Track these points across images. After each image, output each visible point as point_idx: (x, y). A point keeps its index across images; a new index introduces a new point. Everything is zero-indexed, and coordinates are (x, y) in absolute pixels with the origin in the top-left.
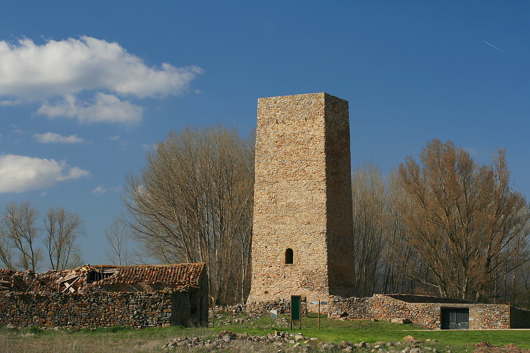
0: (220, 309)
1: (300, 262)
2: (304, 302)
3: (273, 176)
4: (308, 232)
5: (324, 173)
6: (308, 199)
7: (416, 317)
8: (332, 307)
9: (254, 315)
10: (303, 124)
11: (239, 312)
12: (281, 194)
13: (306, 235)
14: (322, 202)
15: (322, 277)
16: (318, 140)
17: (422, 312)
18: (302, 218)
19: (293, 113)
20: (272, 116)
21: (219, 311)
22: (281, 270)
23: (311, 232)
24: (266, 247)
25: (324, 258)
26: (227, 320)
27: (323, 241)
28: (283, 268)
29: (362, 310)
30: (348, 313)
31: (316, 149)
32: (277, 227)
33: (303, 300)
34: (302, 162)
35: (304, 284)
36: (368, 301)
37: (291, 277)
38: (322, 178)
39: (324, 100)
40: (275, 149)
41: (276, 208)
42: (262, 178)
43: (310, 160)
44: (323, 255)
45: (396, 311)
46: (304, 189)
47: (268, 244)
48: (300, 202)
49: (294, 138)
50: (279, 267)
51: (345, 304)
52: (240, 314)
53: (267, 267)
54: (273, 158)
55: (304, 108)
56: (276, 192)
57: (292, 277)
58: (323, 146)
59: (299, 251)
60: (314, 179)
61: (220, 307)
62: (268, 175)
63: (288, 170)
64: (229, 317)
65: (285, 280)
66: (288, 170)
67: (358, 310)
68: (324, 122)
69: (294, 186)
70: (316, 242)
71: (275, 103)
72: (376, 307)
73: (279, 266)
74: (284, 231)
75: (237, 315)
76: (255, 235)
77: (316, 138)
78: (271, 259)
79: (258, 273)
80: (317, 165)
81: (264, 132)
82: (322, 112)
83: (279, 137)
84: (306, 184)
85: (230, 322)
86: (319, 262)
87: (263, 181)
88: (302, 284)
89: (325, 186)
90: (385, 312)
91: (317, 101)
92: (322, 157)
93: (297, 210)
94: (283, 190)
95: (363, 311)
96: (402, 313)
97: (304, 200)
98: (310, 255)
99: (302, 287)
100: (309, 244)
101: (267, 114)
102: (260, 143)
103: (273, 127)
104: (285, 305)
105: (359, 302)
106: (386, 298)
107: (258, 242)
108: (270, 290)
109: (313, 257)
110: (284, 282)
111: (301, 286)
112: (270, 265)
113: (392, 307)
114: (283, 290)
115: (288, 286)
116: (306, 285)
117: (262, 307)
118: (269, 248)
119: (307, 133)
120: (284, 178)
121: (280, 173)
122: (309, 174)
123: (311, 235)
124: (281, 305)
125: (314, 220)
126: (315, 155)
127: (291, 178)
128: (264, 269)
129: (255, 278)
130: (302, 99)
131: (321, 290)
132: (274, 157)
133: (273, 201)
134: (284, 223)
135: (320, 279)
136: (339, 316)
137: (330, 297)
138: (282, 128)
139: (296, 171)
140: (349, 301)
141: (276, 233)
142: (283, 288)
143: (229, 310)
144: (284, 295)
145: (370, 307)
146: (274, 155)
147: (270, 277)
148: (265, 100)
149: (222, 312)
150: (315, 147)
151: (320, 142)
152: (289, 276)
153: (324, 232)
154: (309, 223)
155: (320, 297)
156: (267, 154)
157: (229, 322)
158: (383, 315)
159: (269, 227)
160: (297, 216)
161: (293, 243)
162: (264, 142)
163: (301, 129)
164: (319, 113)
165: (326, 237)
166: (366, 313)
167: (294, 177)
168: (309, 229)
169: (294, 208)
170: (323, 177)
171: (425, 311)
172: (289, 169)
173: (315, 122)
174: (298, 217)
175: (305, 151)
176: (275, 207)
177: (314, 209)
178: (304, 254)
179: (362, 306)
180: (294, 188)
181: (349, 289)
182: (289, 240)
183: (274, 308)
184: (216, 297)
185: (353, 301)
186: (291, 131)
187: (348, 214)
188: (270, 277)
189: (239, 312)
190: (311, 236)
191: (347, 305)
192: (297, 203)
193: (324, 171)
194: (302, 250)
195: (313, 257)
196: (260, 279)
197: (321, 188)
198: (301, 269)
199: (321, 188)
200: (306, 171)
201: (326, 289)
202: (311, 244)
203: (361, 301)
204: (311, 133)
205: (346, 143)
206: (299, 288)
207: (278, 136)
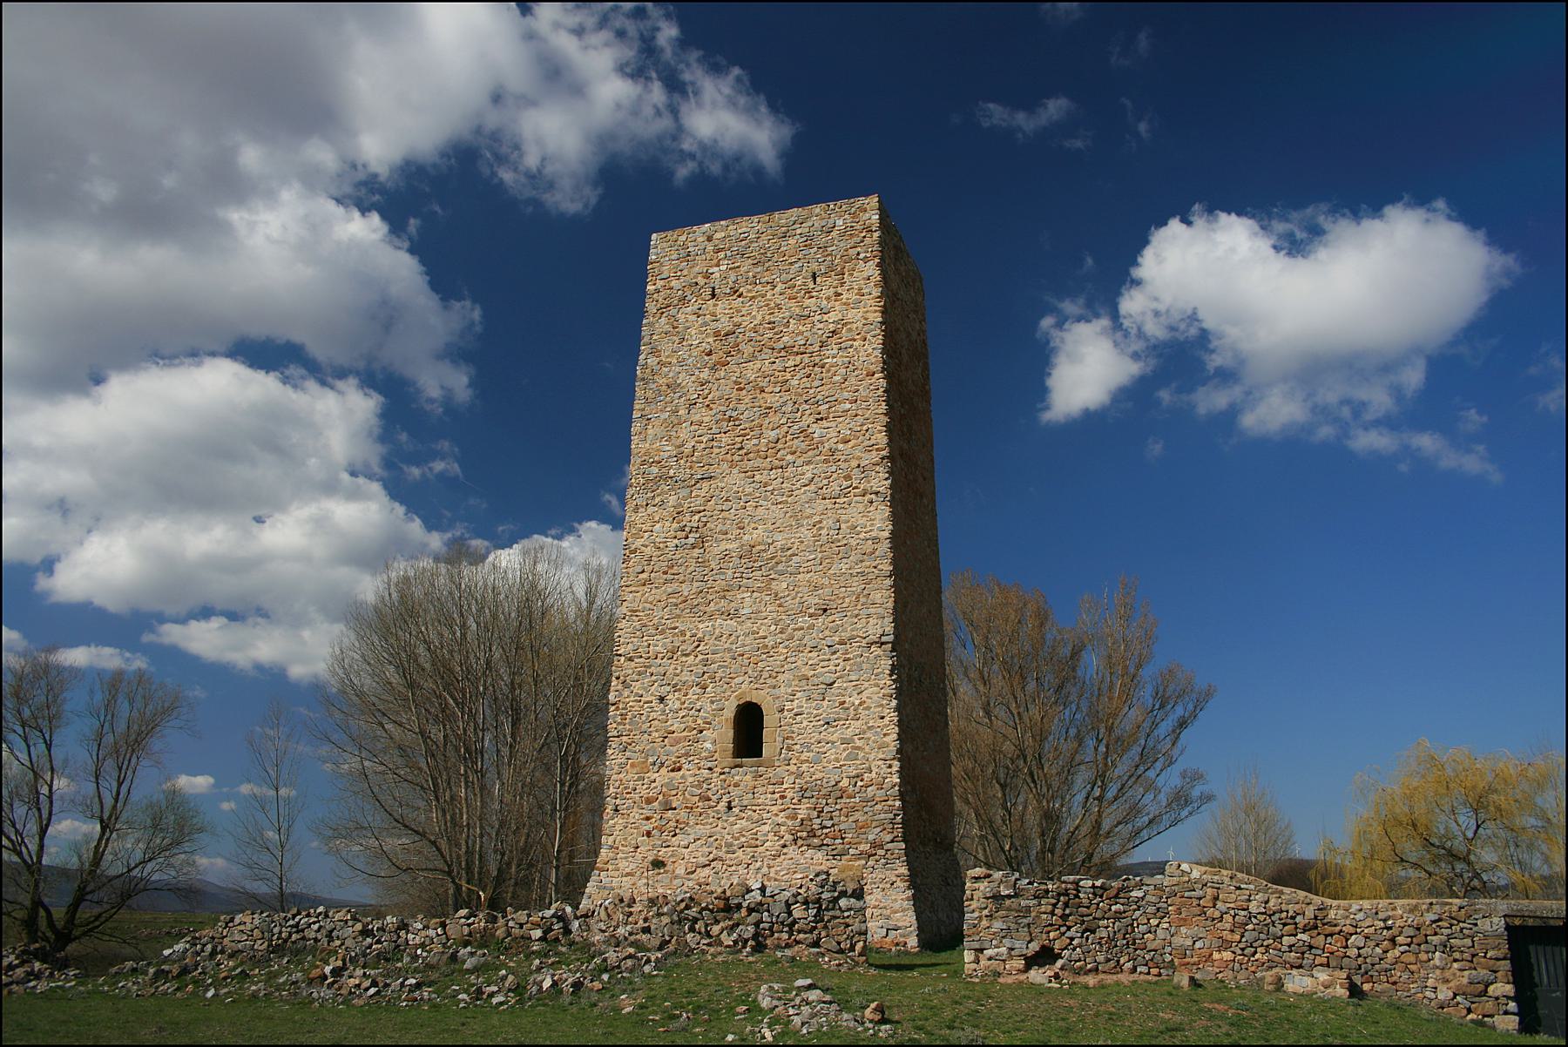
0: (473, 923)
1: (789, 749)
2: (852, 900)
3: (694, 459)
4: (824, 642)
5: (882, 438)
6: (821, 528)
7: (1384, 965)
8: (985, 923)
9: (630, 956)
10: (803, 292)
11: (557, 940)
12: (720, 516)
13: (814, 654)
14: (874, 534)
15: (879, 807)
16: (858, 337)
17: (1412, 942)
18: (799, 595)
19: (770, 263)
20: (695, 277)
21: (470, 934)
22: (716, 780)
23: (834, 640)
24: (662, 699)
25: (885, 735)
26: (504, 978)
27: (881, 673)
28: (724, 773)
29: (1119, 936)
30: (1056, 946)
31: (850, 363)
33: (850, 892)
34: (798, 410)
35: (805, 834)
36: (1140, 894)
37: (754, 808)
38: (875, 456)
39: (877, 217)
40: (705, 375)
41: (703, 562)
42: (655, 470)
43: (827, 400)
44: (880, 723)
45: (1283, 936)
46: (808, 494)
47: (668, 688)
48: (793, 540)
49: (771, 335)
50: (710, 769)
51: (1043, 909)
52: (564, 949)
53: (664, 771)
54: (695, 404)
55: (806, 246)
56: (705, 510)
57: (758, 808)
58: (877, 353)
59: (786, 713)
60: (845, 461)
61: (475, 916)
62: (675, 459)
63: (749, 437)
64: (512, 964)
65: (732, 819)
66: (749, 437)
67: (1104, 934)
68: (878, 279)
69: (770, 488)
70: (853, 678)
71: (710, 239)
72: (1185, 920)
73: (709, 765)
74: (729, 641)
75: (546, 955)
76: (623, 659)
77: (850, 330)
78: (678, 741)
79: (627, 793)
80: (856, 416)
81: (668, 328)
82: (872, 251)
83: (719, 338)
84: (813, 478)
85: (518, 989)
86: (867, 749)
87: (658, 479)
88: (799, 834)
89: (886, 479)
90: (1225, 945)
91: (852, 222)
92: (872, 387)
93: (780, 567)
94: (731, 503)
95: (1124, 938)
96: (1311, 947)
97: (806, 532)
98: (828, 723)
99: (796, 844)
100: (825, 686)
101: (679, 274)
102: (652, 361)
103: (700, 309)
104: (769, 911)
105: (1101, 896)
106: (1227, 880)
107: (634, 684)
108: (672, 855)
109: (842, 733)
110: (725, 825)
112: (675, 763)
113: (1261, 917)
114: (720, 854)
115: (743, 839)
116: (815, 836)
117: (665, 920)
118: (673, 702)
119: (819, 317)
120: (732, 464)
121: (720, 447)
122: (826, 445)
123: (835, 653)
124: (750, 910)
125: (844, 598)
126: (846, 383)
127: (758, 463)
128: (652, 778)
129: (616, 810)
130: (800, 221)
131: (876, 854)
132: (700, 400)
133: (691, 540)
134: (732, 612)
136: (1021, 963)
137: (975, 878)
138: (731, 308)
139: (779, 439)
140: (1059, 895)
141: (698, 649)
142: (724, 849)
143: (516, 931)
144: (727, 874)
145: (1154, 922)
146: (701, 393)
147: (675, 809)
148: (675, 236)
149: (483, 940)
150: (848, 357)
151: (867, 342)
152: (745, 803)
153: (884, 639)
154: (825, 610)
155: (871, 883)
156: (675, 393)
157: (510, 990)
158: (1216, 956)
159: (675, 628)
160: (781, 586)
161: (762, 681)
162: (667, 357)
163: (797, 306)
164: (862, 256)
165: (893, 657)
166: (1136, 950)
167: (769, 459)
168: (827, 633)
169: (767, 559)
170: (877, 450)
171: (1426, 936)
172: (752, 433)
173: (845, 283)
174: (782, 592)
175: (810, 374)
176: (700, 560)
177: (845, 561)
178: (805, 723)
179: (1118, 916)
180: (769, 494)
182: (750, 672)
183: (722, 924)
184: (490, 890)
185: (1077, 896)
186: (759, 317)
188: (675, 809)
189: (558, 938)
190: (835, 656)
191: (1053, 913)
192: (780, 543)
193: (880, 432)
194: (798, 707)
195: (842, 733)
196: (636, 815)
197: (872, 487)
198: (793, 777)
199: (872, 487)
200: (815, 435)
202: (832, 684)
203: (1113, 892)
204: (833, 317)
206: (784, 846)
207: (717, 334)
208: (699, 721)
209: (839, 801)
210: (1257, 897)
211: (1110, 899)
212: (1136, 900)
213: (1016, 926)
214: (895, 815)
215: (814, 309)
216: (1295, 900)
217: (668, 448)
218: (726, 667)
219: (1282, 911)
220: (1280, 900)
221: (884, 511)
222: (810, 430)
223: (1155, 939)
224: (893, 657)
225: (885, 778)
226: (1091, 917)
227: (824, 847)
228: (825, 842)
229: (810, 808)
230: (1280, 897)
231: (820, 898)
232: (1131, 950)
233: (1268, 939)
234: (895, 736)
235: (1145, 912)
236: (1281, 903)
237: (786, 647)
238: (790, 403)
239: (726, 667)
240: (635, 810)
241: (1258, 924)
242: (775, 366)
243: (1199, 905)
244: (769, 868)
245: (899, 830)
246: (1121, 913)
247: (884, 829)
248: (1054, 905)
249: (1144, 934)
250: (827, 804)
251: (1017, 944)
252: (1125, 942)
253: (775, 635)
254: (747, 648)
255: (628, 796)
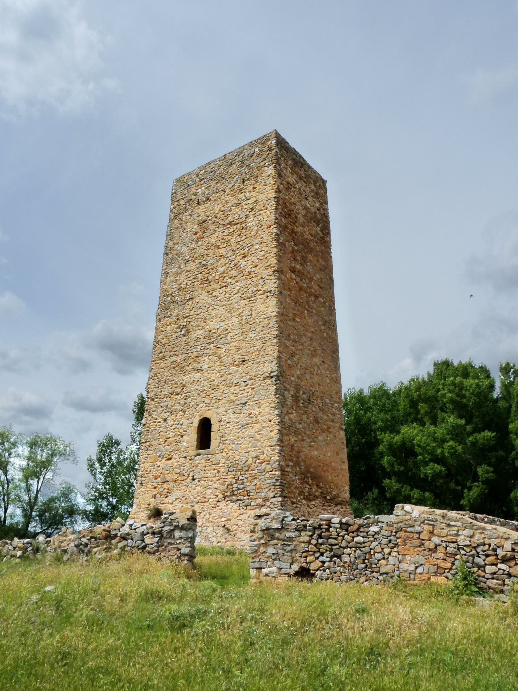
8: (262, 549)
13: (237, 387)
15: (267, 475)
24: (165, 420)
29: (360, 561)
32: (186, 379)
37: (205, 479)
42: (169, 299)
50: (185, 457)
51: (302, 539)
53: (164, 460)
58: (273, 215)
59: (222, 422)
70: (256, 399)
73: (185, 455)
95: (364, 563)
100: (242, 405)
106: (440, 518)
107: (153, 413)
110: (190, 489)
111: (224, 497)
112: (169, 455)
115: (199, 498)
116: (234, 495)
121: (198, 281)
123: (247, 385)
128: (159, 464)
135: (263, 480)
147: (168, 482)
153: (272, 374)
154: (244, 361)
166: (372, 572)
168: (244, 374)
177: (253, 332)
179: (358, 546)
181: (336, 508)
182: (206, 401)
185: (328, 530)
187: (330, 358)
190: (247, 387)
193: (273, 257)
200: (242, 266)
201: (276, 503)
205: (323, 238)
208: (181, 431)
209: (247, 473)
210: (464, 532)
211: (353, 532)
212: (374, 533)
213: (282, 552)
214: (276, 480)
215: (243, 199)
216: (496, 535)
217: (175, 286)
218: (195, 399)
219: (484, 545)
220: (483, 535)
221: (273, 302)
222: (239, 264)
223: (387, 565)
224: (277, 384)
225: (271, 457)
226: (337, 546)
227: (238, 502)
228: (239, 498)
229: (232, 478)
230: (483, 533)
231: (162, 530)
232: (368, 573)
233: (474, 567)
234: (277, 431)
235: (379, 543)
236: (484, 538)
237: (223, 385)
238: (231, 251)
239: (195, 399)
240: (150, 483)
241: (465, 555)
242: (224, 234)
243: (419, 538)
244: (210, 515)
245: (278, 490)
246: (360, 544)
247: (270, 489)
248: (311, 536)
249: (379, 560)
250: (241, 475)
251: (284, 565)
252: (363, 566)
253: (219, 378)
254: (205, 388)
255: (147, 475)
